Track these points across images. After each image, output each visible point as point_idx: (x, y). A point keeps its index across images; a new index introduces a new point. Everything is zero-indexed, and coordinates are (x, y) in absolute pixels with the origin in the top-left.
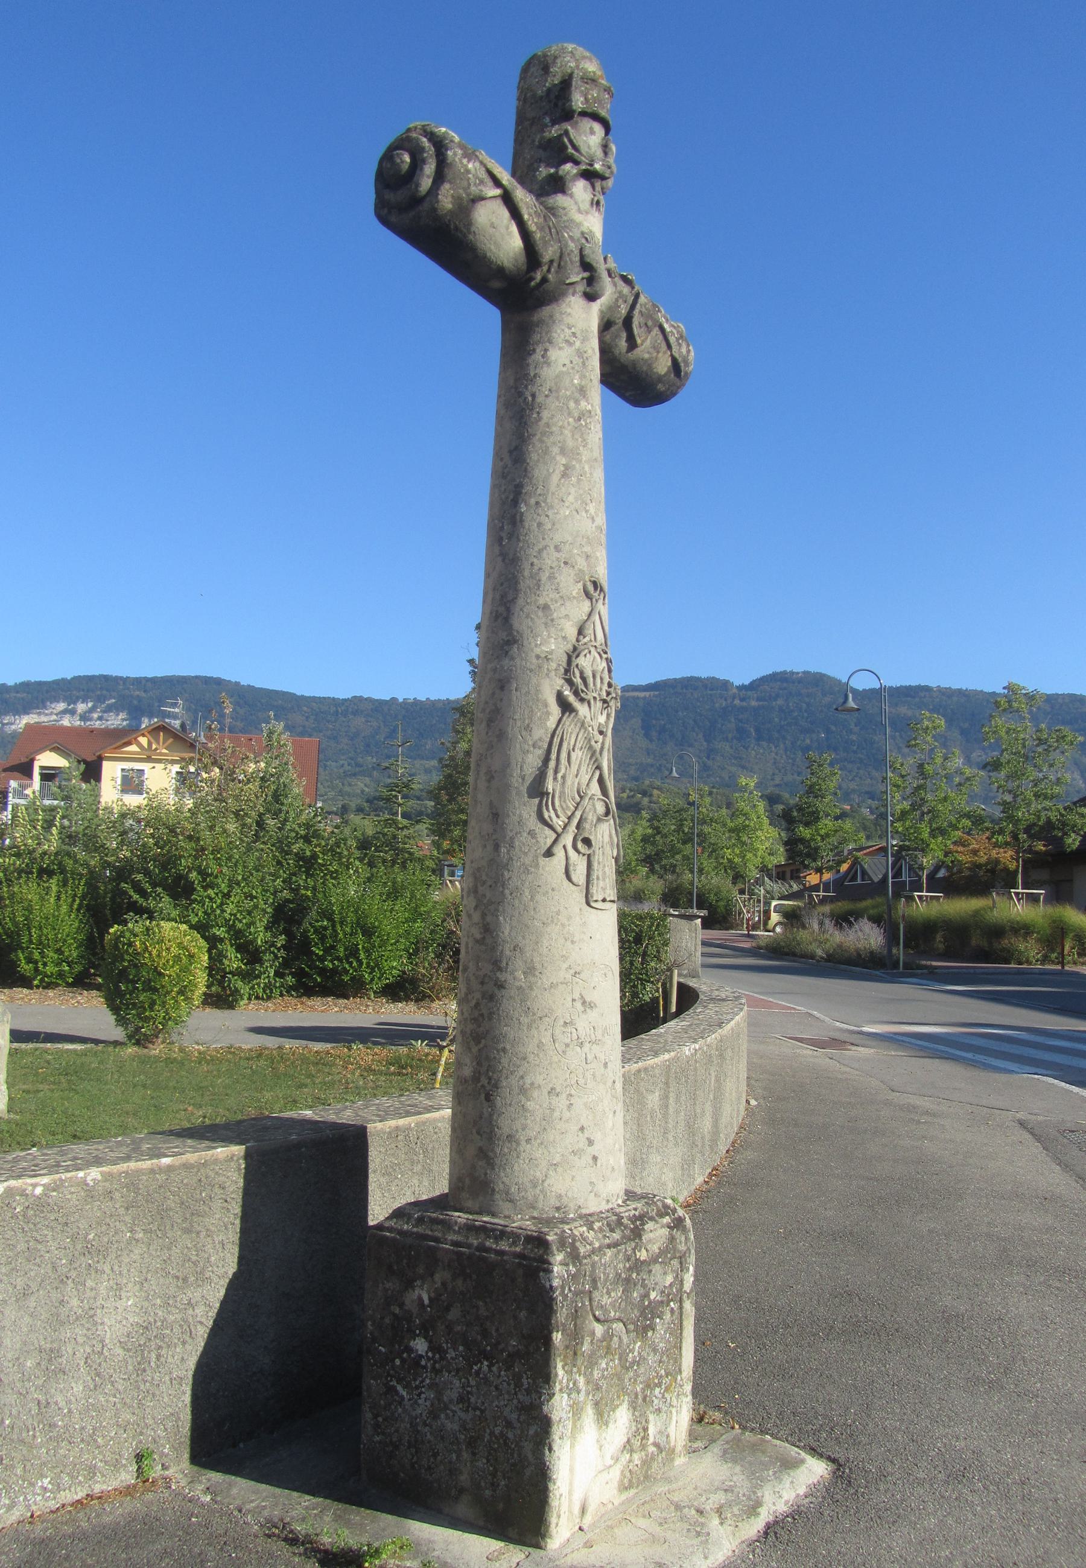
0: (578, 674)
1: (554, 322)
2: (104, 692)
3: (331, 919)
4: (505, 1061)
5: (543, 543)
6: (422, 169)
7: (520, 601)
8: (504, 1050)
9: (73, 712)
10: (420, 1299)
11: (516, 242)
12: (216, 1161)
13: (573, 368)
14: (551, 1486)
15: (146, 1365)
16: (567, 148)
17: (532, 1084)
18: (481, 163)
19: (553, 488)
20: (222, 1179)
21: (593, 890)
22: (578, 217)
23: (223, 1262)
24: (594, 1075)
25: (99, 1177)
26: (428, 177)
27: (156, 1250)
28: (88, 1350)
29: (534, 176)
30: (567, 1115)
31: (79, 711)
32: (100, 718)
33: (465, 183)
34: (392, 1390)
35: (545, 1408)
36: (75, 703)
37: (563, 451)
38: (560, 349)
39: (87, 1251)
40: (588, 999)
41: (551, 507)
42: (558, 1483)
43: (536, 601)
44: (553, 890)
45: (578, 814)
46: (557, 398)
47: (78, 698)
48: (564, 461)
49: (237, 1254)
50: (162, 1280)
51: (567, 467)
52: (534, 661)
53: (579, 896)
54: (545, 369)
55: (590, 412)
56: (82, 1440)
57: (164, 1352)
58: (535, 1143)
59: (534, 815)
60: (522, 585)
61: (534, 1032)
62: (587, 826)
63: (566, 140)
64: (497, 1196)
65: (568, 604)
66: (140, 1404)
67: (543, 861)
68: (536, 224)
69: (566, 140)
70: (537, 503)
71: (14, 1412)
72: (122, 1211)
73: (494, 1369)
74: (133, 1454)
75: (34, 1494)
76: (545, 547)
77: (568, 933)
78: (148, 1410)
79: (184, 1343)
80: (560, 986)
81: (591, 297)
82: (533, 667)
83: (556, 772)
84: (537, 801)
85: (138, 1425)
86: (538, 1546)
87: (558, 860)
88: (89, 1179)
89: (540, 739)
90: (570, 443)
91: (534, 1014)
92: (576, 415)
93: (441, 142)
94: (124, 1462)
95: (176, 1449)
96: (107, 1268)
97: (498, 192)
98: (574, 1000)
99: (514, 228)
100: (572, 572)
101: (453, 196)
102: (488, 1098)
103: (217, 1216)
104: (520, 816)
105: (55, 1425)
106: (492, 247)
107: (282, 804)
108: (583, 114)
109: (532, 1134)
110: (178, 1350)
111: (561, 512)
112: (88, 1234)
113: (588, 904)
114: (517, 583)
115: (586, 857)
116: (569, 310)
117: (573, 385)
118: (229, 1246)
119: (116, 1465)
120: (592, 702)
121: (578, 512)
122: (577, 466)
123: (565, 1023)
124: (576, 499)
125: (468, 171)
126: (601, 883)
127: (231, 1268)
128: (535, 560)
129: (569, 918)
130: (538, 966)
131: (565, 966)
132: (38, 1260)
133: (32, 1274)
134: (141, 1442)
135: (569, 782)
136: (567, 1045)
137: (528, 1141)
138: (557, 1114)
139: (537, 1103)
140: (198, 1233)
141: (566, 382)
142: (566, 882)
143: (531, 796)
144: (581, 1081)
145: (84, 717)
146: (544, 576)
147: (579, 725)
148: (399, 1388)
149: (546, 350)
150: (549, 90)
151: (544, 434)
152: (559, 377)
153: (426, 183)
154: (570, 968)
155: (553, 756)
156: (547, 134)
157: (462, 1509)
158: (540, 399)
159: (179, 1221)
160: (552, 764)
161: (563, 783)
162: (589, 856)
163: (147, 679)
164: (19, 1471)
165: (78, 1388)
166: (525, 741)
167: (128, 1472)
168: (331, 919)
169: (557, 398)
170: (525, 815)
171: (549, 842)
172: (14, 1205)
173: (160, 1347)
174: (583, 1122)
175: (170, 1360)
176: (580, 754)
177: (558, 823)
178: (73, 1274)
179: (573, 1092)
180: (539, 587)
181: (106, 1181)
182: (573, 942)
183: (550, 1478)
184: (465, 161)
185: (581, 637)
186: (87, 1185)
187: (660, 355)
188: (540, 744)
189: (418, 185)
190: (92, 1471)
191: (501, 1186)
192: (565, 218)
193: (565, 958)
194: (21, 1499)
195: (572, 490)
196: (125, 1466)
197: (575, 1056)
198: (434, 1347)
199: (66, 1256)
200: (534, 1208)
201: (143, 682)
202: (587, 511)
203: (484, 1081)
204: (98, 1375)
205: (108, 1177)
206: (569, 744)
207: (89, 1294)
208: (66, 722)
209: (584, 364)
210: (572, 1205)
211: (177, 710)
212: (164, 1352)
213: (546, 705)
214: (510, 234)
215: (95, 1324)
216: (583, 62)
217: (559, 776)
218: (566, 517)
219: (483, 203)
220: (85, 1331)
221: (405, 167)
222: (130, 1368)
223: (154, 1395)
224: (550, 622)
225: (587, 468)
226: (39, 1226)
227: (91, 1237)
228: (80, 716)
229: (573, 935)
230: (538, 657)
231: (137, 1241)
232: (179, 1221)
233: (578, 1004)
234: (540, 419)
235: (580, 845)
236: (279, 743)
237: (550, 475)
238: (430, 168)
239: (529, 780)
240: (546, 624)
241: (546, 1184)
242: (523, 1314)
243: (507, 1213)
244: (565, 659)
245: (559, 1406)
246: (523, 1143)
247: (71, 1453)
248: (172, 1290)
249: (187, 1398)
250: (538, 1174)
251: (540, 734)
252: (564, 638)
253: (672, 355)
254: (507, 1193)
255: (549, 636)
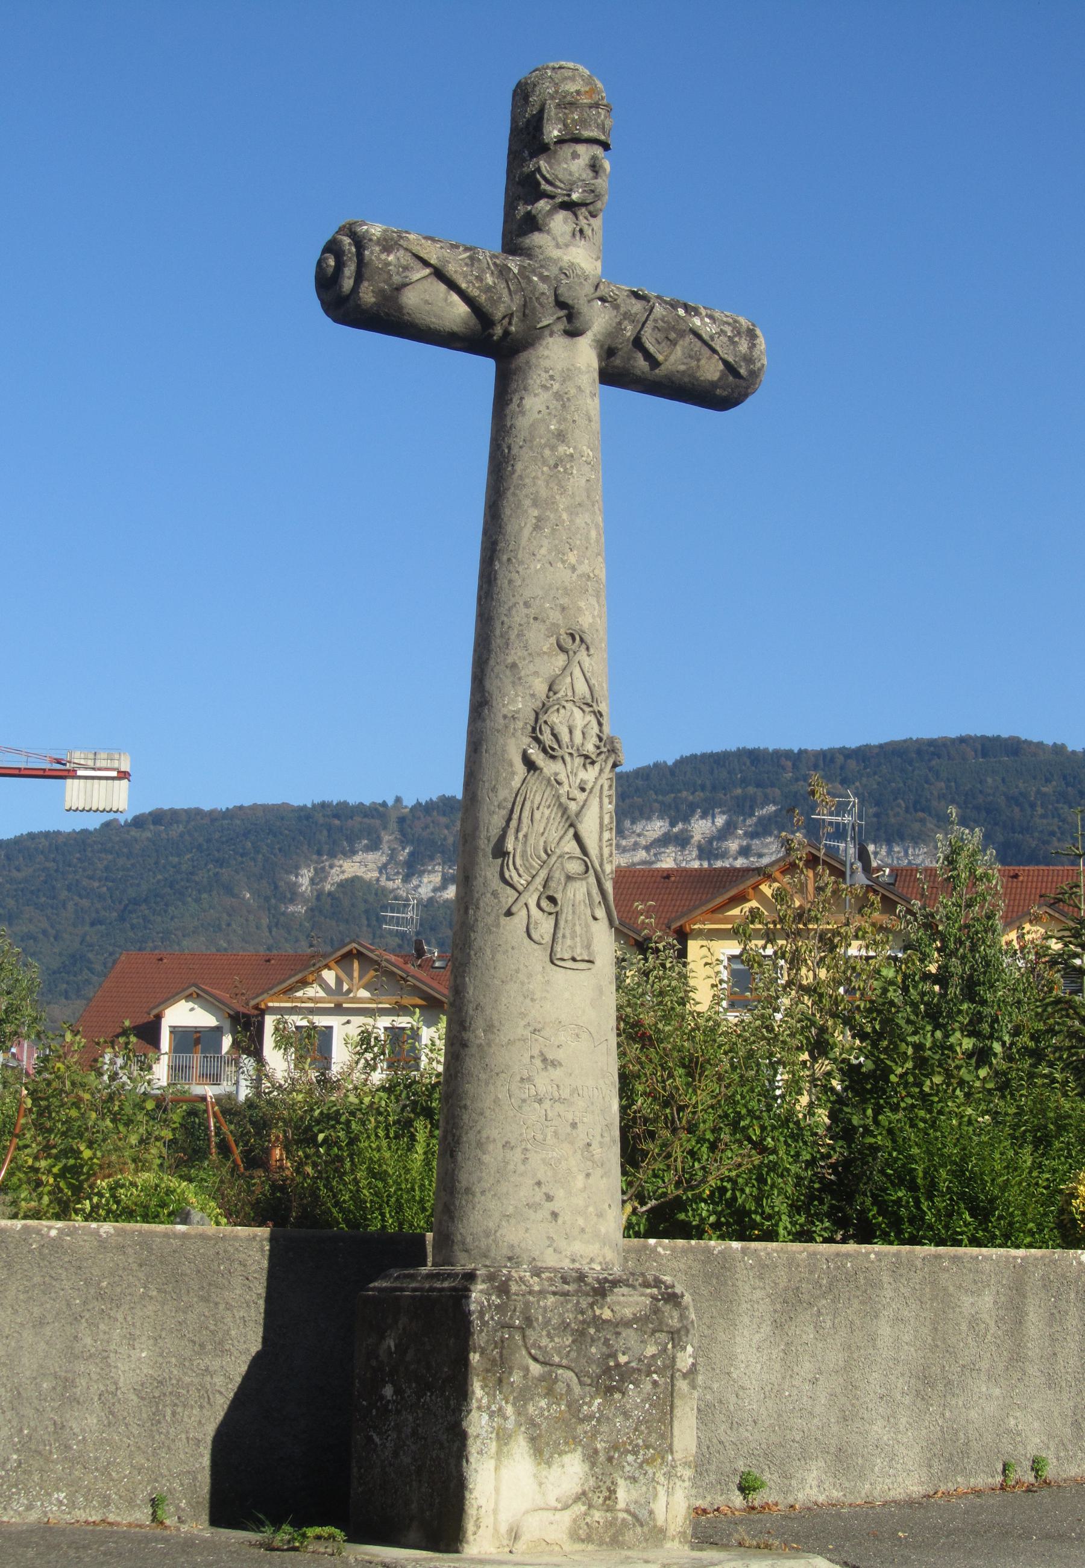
0: (549, 731)
1: (530, 368)
2: (751, 790)
3: (913, 1187)
4: (465, 1117)
5: (513, 600)
6: (343, 272)
7: (492, 662)
8: (465, 1107)
9: (682, 841)
10: (389, 1347)
11: (461, 309)
12: (236, 1238)
13: (550, 414)
14: (467, 1495)
15: (161, 1417)
16: (539, 184)
17: (488, 1138)
18: (406, 249)
19: (524, 542)
20: (242, 1256)
21: (558, 948)
22: (555, 253)
23: (246, 1339)
24: (556, 1133)
25: (112, 1231)
26: (349, 278)
27: (171, 1311)
28: (102, 1388)
29: (514, 215)
30: (521, 1168)
31: (697, 837)
32: (745, 852)
33: (386, 276)
34: (370, 1439)
35: (464, 1424)
36: (686, 819)
37: (535, 504)
38: (536, 395)
39: (100, 1296)
40: (550, 1057)
41: (521, 563)
42: (475, 1494)
43: (505, 660)
44: (513, 948)
45: (543, 874)
46: (531, 448)
47: (692, 808)
48: (536, 513)
49: (261, 1334)
50: (176, 1341)
51: (539, 519)
52: (502, 721)
53: (539, 956)
54: (520, 418)
55: (572, 455)
56: (97, 1469)
57: (179, 1410)
58: (489, 1195)
59: (497, 876)
60: (494, 645)
61: (491, 1088)
62: (552, 884)
63: (538, 176)
64: (456, 1247)
65: (537, 660)
66: (155, 1453)
67: (504, 920)
68: (478, 288)
69: (538, 176)
70: (509, 560)
71: (32, 1424)
72: (135, 1267)
73: (433, 1397)
74: (148, 1498)
75: (51, 1504)
76: (515, 605)
77: (528, 990)
78: (163, 1461)
79: (201, 1407)
80: (517, 1043)
81: (573, 333)
82: (500, 727)
83: (518, 831)
84: (500, 861)
85: (153, 1472)
86: (457, 1551)
87: (519, 921)
88: (102, 1231)
89: (505, 800)
90: (544, 493)
91: (492, 1071)
92: (552, 463)
93: (360, 242)
94: (138, 1502)
95: (194, 1507)
96: (120, 1316)
97: (428, 271)
98: (532, 1057)
99: (455, 297)
100: (543, 627)
101: (373, 291)
102: (452, 1156)
103: (238, 1292)
104: (485, 877)
105: (71, 1448)
106: (433, 320)
107: (983, 1002)
108: (561, 141)
109: (487, 1185)
110: (194, 1412)
111: (532, 567)
112: (100, 1282)
113: (552, 962)
114: (489, 644)
115: (553, 916)
116: (546, 353)
117: (549, 431)
118: (252, 1324)
119: (131, 1503)
120: (568, 758)
121: (567, 562)
122: (552, 516)
123: (522, 1079)
124: (549, 551)
125: (389, 264)
126: (569, 942)
127: (255, 1346)
128: (505, 619)
129: (530, 976)
130: (496, 1023)
131: (523, 1023)
132: (53, 1295)
133: (48, 1306)
134: (156, 1488)
135: (531, 841)
136: (524, 1101)
137: (483, 1193)
138: (511, 1167)
139: (492, 1157)
140: (216, 1304)
141: (542, 430)
142: (527, 940)
143: (495, 857)
144: (539, 1137)
145: (706, 851)
146: (513, 635)
147: (545, 782)
148: (375, 1437)
149: (522, 399)
150: (528, 121)
151: (517, 487)
152: (533, 426)
153: (348, 284)
154: (529, 1024)
155: (515, 816)
156: (525, 169)
157: (413, 1535)
158: (515, 451)
159: (196, 1288)
160: (514, 823)
161: (525, 842)
162: (557, 913)
163: (848, 754)
164: (36, 1478)
165: (93, 1420)
166: (492, 803)
167: (143, 1513)
168: (913, 1187)
169: (531, 448)
170: (489, 874)
171: (511, 901)
172: (31, 1241)
173: (175, 1405)
174: (540, 1176)
175: (186, 1419)
176: (547, 812)
177: (520, 882)
178: (87, 1315)
179: (529, 1146)
180: (508, 645)
181: (119, 1235)
182: (533, 1000)
183: (466, 1488)
184: (383, 256)
185: (551, 694)
186: (100, 1236)
187: (703, 362)
188: (505, 804)
189: (341, 287)
190: (106, 1502)
191: (459, 1237)
192: (541, 257)
193: (523, 1015)
194: (39, 1503)
195: (545, 542)
196: (140, 1506)
197: (534, 1113)
198: (398, 1391)
199: (80, 1297)
200: (486, 1257)
201: (840, 759)
202: (563, 562)
203: (450, 1138)
204: (112, 1413)
205: (119, 1233)
206: (532, 802)
207: (101, 1336)
208: (668, 862)
209: (564, 406)
210: (525, 1256)
211: (847, 819)
212: (179, 1410)
213: (511, 765)
214: (451, 304)
215: (109, 1366)
216: (575, 77)
217: (521, 835)
218: (537, 571)
219: (410, 287)
220: (98, 1370)
221: (330, 270)
222: (145, 1416)
223: (169, 1448)
224: (518, 680)
225: (565, 516)
226: (54, 1264)
227: (104, 1284)
228: (700, 848)
229: (533, 993)
230: (505, 717)
231: (151, 1298)
232: (196, 1288)
233: (538, 1062)
234: (513, 472)
235: (544, 903)
236: (972, 873)
237: (521, 529)
238: (349, 270)
239: (494, 840)
240: (513, 683)
241: (498, 1234)
242: (452, 1341)
243: (463, 1262)
244: (533, 717)
245: (478, 1423)
246: (478, 1195)
247: (86, 1478)
248: (188, 1353)
249: (206, 1461)
250: (491, 1224)
251: (504, 794)
252: (533, 695)
253: (721, 358)
254: (463, 1243)
255: (517, 695)
